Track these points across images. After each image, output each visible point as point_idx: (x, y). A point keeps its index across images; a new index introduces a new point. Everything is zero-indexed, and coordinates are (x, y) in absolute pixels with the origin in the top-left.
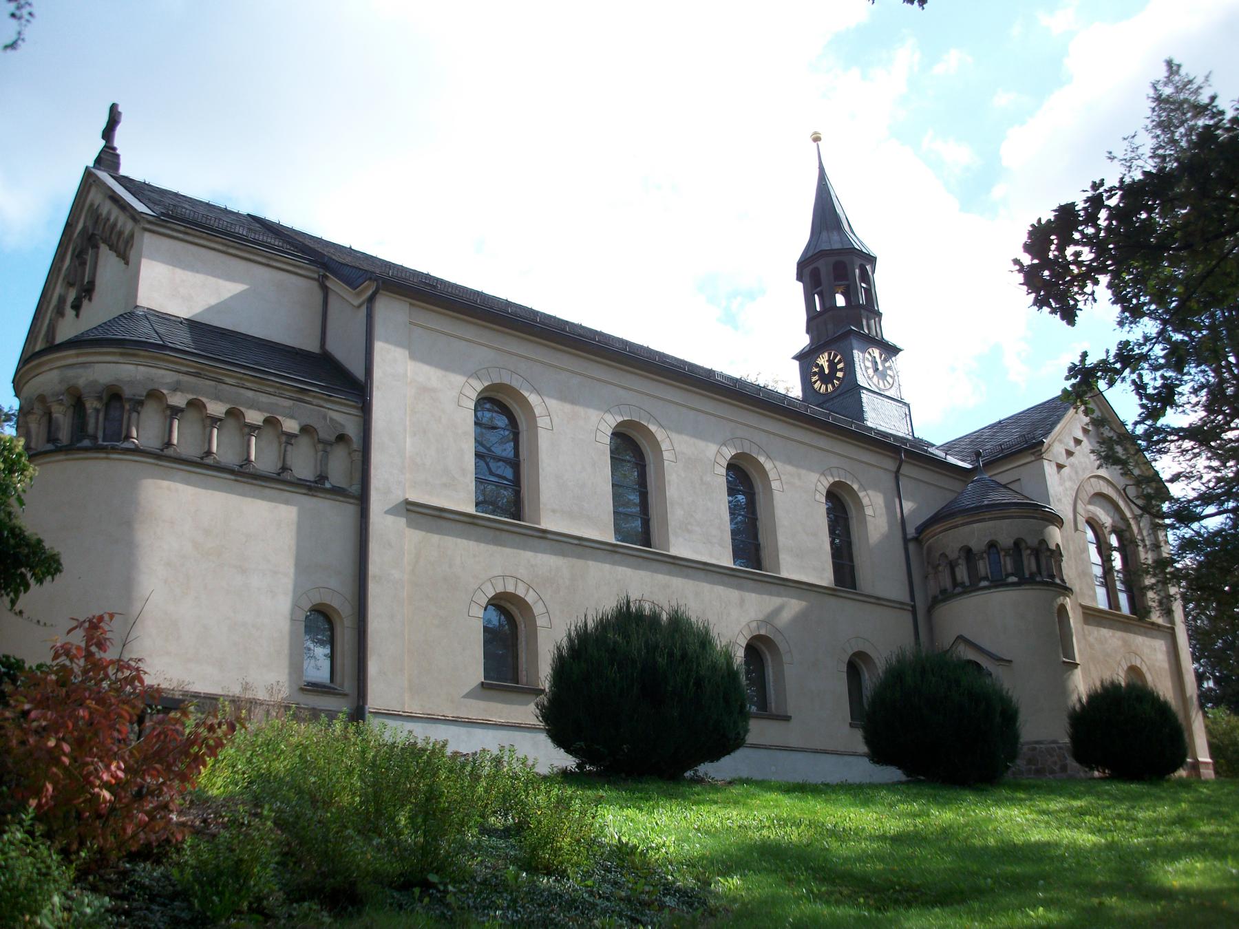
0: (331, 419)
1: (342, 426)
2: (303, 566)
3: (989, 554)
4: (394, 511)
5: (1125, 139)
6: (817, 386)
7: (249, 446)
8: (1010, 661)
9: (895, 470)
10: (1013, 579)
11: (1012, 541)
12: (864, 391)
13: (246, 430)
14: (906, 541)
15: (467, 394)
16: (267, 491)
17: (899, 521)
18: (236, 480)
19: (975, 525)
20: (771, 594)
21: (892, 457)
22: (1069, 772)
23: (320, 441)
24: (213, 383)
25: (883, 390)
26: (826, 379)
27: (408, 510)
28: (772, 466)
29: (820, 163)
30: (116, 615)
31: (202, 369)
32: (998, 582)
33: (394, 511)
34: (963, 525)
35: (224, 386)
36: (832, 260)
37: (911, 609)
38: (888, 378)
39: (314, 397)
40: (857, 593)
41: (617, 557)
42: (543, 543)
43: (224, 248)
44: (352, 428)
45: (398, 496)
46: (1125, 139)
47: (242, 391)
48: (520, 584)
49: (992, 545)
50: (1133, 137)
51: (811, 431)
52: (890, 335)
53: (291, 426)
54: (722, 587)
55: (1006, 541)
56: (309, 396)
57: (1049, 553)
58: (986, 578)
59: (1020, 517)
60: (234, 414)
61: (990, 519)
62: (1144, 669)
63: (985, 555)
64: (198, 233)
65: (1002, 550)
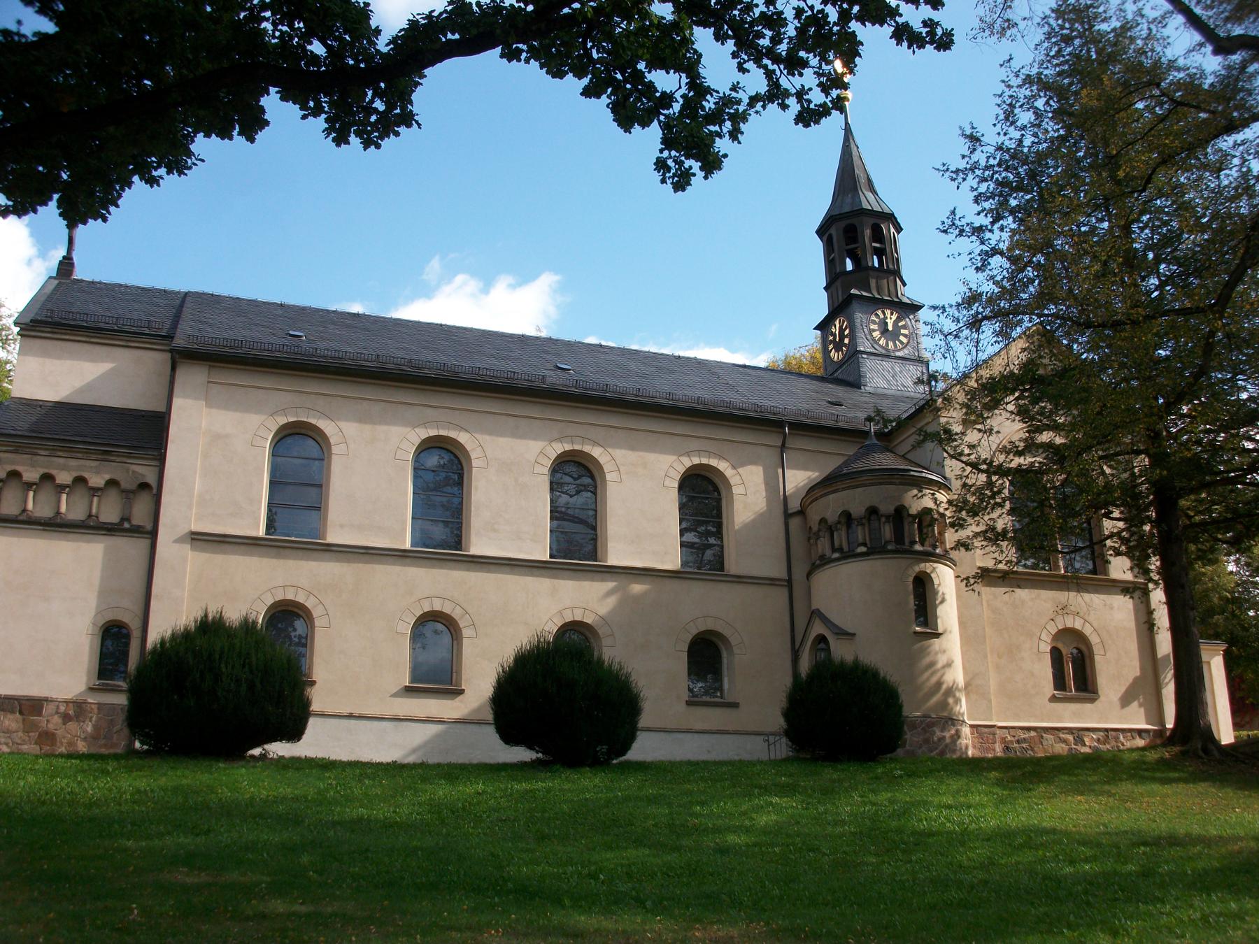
0: (134, 472)
1: (143, 476)
2: (103, 593)
3: (869, 520)
4: (180, 540)
5: (1001, 65)
6: (832, 354)
7: (59, 501)
8: (854, 635)
9: (780, 444)
10: (863, 549)
11: (863, 510)
12: (865, 356)
13: (59, 489)
14: (787, 515)
15: (261, 435)
16: (71, 536)
17: (782, 497)
18: (44, 530)
19: (831, 496)
20: (603, 580)
21: (777, 432)
22: (908, 747)
23: (123, 491)
24: (30, 456)
25: (894, 351)
26: (838, 347)
27: (192, 539)
28: (609, 458)
29: (847, 123)
30: (302, 619)
31: (20, 446)
32: (848, 555)
33: (180, 540)
34: (822, 496)
35: (39, 457)
36: (843, 224)
37: (786, 584)
38: (902, 338)
39: (118, 456)
40: (726, 575)
41: (408, 560)
42: (327, 555)
43: (88, 339)
44: (151, 479)
45: (184, 529)
46: (1001, 65)
47: (55, 459)
48: (300, 591)
49: (873, 511)
50: (1009, 61)
51: (664, 418)
52: (910, 293)
53: (97, 480)
54: (531, 578)
55: (858, 510)
56: (113, 456)
57: (910, 519)
58: (865, 544)
59: (873, 485)
60: (47, 478)
61: (844, 489)
62: (1088, 631)
63: (864, 521)
64: (64, 331)
65: (882, 516)
